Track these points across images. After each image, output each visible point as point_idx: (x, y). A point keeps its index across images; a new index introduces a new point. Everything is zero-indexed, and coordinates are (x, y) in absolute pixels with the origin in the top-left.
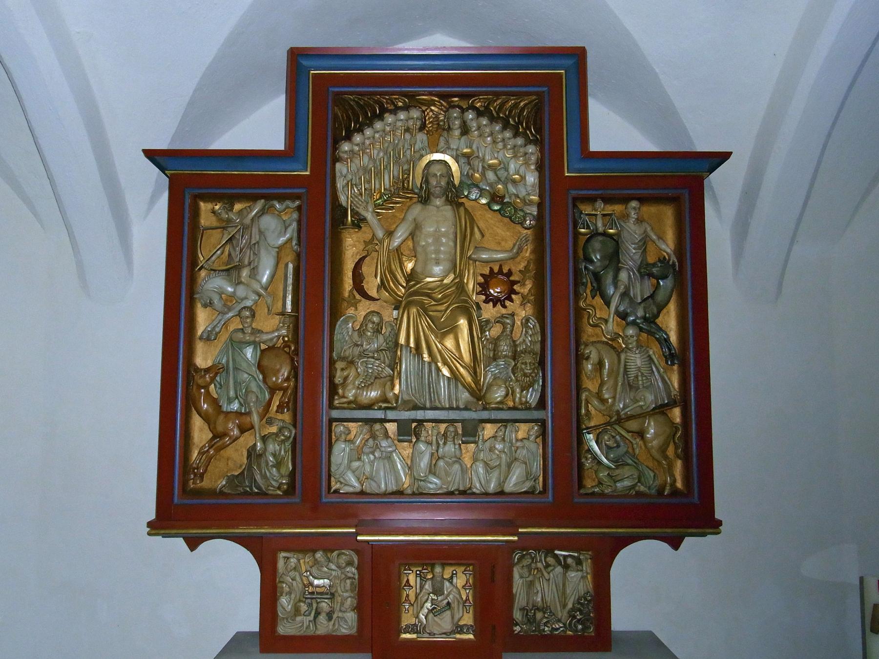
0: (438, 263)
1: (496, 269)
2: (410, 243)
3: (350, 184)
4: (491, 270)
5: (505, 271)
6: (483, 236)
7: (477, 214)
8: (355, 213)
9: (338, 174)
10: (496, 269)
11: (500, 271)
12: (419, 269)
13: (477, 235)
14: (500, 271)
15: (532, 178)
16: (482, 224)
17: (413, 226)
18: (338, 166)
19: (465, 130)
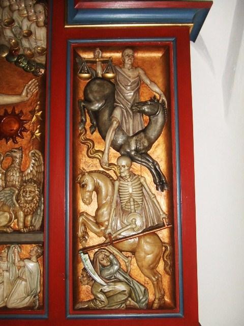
1: (10, 111)
10: (10, 111)
15: (41, 34)
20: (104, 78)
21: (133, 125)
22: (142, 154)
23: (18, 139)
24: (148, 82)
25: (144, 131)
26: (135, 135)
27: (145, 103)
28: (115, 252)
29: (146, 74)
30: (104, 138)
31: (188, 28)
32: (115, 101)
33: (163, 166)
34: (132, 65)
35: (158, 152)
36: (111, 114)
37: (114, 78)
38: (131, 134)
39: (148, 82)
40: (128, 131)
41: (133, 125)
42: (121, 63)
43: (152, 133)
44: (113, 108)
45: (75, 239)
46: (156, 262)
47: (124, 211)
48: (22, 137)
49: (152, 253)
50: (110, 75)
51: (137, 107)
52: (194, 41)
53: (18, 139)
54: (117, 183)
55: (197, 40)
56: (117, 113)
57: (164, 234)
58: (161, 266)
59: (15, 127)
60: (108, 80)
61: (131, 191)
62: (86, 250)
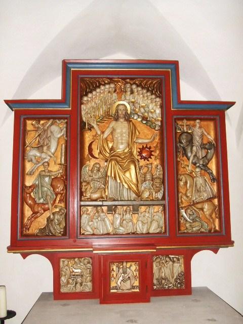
0: (122, 143)
1: (145, 146)
2: (111, 136)
3: (87, 113)
4: (143, 146)
5: (148, 147)
6: (139, 133)
7: (137, 125)
8: (89, 125)
9: (82, 109)
10: (145, 146)
11: (146, 147)
12: (115, 146)
13: (137, 133)
14: (146, 147)
15: (158, 111)
16: (139, 129)
17: (112, 130)
18: (82, 106)
19: (132, 92)
20: (187, 132)
21: (201, 154)
22: (205, 167)
23: (149, 159)
24: (206, 134)
25: (206, 156)
26: (203, 158)
27: (206, 144)
28: (195, 209)
29: (205, 131)
30: (189, 159)
31: (169, 71)
32: (193, 143)
33: (214, 172)
34: (199, 127)
35: (213, 166)
36: (192, 149)
37: (192, 133)
38: (201, 158)
39: (206, 134)
40: (199, 156)
41: (201, 154)
42: (194, 126)
43: (209, 156)
44: (192, 147)
45: (178, 205)
46: (212, 213)
47: (198, 191)
48: (151, 158)
49: (206, 230)
50: (189, 131)
51: (203, 146)
52: (101, 303)
53: (149, 159)
54: (195, 179)
55: (105, 306)
56: (194, 148)
57: (216, 201)
58: (214, 216)
59: (144, 155)
60: (189, 133)
61: (201, 182)
62: (182, 208)
